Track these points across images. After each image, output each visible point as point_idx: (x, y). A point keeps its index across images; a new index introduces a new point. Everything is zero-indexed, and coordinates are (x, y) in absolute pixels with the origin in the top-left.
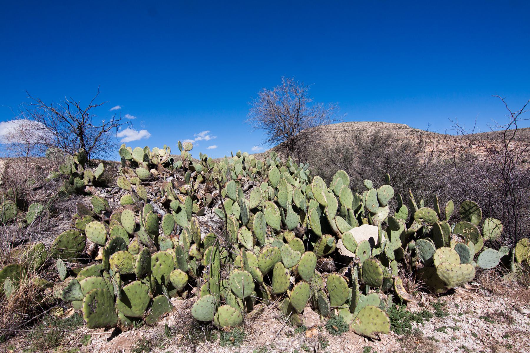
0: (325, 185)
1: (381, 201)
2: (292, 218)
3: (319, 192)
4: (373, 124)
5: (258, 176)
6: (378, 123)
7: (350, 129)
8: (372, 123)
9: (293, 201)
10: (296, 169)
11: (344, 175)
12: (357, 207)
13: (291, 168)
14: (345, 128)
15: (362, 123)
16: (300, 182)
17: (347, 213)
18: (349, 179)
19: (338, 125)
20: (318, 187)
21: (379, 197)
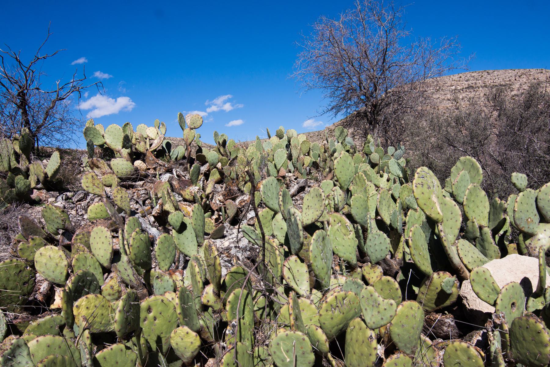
0: (437, 182)
1: (544, 212)
2: (377, 242)
3: (426, 195)
4: (522, 74)
5: (314, 171)
6: (533, 71)
7: (480, 83)
8: (522, 71)
9: (377, 213)
10: (381, 158)
11: (473, 165)
12: (496, 223)
13: (372, 156)
14: (470, 82)
15: (501, 72)
16: (388, 180)
17: (478, 234)
18: (481, 171)
19: (456, 77)
20: (425, 186)
21: (541, 204)
